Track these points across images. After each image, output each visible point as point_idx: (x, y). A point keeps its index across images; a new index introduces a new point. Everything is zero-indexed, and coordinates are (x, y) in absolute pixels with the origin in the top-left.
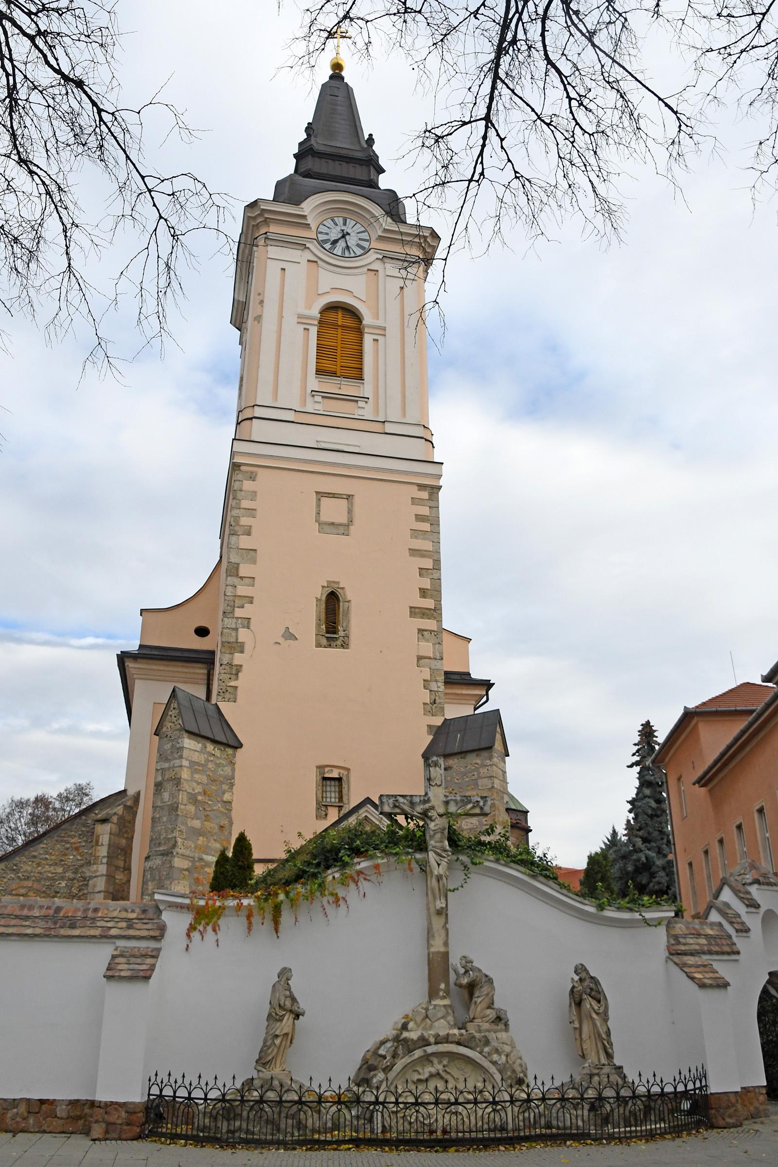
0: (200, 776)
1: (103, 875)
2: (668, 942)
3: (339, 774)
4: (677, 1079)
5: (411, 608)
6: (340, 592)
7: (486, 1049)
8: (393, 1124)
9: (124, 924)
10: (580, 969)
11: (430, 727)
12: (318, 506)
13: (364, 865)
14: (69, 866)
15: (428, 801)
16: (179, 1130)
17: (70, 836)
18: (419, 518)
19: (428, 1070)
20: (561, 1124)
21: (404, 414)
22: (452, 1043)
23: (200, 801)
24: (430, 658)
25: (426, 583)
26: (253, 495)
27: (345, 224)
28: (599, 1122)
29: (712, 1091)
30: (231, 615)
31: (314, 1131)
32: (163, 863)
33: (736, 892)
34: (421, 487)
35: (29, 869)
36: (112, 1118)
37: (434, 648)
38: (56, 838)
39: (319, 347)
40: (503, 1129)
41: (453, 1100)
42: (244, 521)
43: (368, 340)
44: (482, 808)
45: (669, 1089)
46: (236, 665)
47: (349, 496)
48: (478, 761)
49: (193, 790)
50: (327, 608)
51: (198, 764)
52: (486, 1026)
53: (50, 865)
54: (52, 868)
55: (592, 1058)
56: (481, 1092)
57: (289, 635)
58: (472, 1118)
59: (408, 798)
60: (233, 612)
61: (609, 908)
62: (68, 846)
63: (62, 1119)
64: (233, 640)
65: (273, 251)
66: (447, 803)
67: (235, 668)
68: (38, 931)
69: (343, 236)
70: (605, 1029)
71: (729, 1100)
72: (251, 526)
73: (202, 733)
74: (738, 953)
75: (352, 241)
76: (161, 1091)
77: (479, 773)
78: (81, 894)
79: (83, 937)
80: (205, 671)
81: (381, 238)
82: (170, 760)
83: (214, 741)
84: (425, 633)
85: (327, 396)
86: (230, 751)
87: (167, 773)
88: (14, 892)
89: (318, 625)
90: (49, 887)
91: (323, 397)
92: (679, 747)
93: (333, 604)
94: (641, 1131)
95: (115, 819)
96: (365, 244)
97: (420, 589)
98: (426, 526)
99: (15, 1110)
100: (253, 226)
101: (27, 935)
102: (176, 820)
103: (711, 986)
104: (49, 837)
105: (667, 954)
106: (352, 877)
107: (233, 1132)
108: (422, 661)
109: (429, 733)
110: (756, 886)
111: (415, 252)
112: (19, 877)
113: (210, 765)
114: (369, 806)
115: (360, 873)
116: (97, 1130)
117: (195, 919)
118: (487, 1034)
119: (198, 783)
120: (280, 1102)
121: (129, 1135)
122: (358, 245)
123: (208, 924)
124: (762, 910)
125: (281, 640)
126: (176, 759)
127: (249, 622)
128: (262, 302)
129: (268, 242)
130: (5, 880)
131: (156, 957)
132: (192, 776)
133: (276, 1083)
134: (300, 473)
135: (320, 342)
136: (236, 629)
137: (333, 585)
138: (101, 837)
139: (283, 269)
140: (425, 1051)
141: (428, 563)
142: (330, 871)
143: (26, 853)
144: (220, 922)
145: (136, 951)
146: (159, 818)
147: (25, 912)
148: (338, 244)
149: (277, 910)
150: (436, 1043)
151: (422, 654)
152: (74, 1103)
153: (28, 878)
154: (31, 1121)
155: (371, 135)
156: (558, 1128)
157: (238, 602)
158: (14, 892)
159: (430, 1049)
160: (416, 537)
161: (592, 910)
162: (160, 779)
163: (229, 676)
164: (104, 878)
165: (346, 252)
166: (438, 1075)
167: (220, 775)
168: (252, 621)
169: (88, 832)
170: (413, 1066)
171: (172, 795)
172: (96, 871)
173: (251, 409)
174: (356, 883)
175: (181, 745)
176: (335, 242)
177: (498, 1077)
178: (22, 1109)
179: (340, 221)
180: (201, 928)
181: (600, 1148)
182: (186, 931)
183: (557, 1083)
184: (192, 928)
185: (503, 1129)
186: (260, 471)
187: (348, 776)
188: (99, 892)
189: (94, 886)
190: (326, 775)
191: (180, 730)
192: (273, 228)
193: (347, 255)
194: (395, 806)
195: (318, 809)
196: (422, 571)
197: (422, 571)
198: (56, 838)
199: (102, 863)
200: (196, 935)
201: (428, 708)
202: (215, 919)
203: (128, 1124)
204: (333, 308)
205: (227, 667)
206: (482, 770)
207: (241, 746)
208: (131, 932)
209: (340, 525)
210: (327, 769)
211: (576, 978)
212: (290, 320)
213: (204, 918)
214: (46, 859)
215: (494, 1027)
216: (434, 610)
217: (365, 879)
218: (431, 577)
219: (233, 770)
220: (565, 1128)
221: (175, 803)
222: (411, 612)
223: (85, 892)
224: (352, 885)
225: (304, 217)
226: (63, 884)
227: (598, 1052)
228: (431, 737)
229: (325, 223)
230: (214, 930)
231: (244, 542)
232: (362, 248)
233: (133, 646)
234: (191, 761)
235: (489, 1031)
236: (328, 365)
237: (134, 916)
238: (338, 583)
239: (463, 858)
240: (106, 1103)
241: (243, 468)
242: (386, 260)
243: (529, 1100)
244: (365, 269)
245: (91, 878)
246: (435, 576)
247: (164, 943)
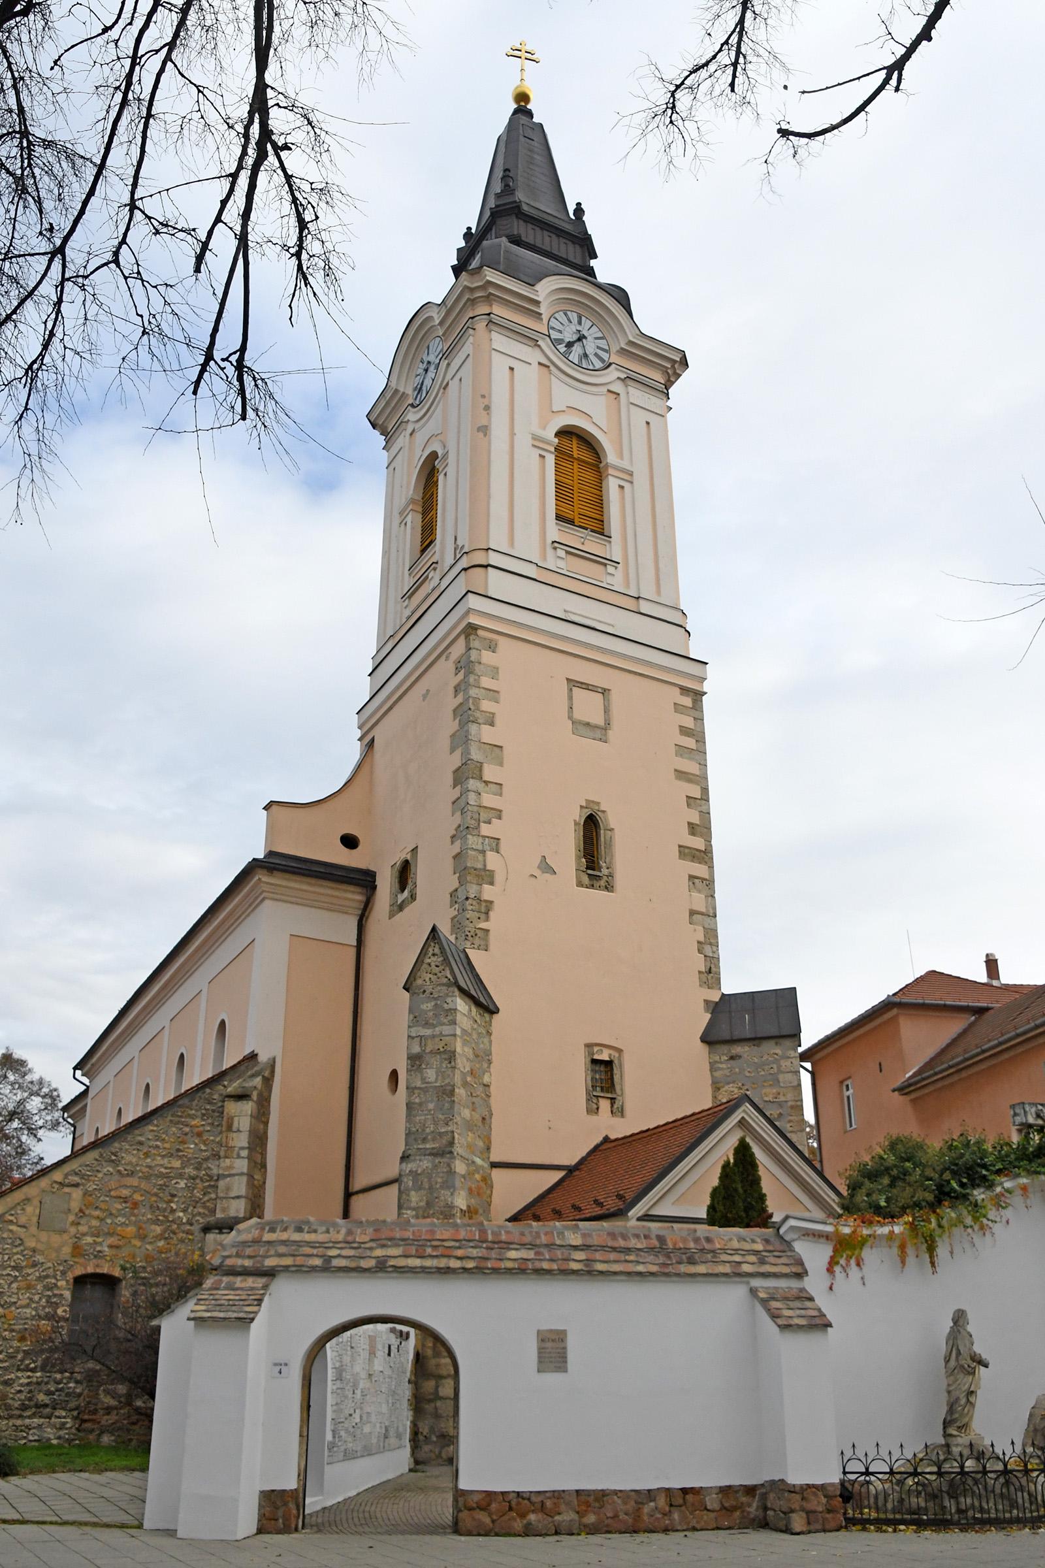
1: (242, 1174)
3: (610, 1056)
5: (680, 846)
9: (753, 1258)
12: (570, 698)
14: (189, 1159)
17: (190, 1116)
18: (684, 731)
21: (659, 592)
24: (702, 914)
25: (695, 818)
26: (494, 672)
27: (580, 323)
30: (475, 832)
32: (435, 1166)
34: (684, 690)
38: (170, 1118)
39: (558, 483)
42: (486, 705)
43: (612, 485)
46: (486, 901)
47: (605, 690)
48: (778, 1051)
53: (163, 1157)
54: (166, 1160)
57: (546, 867)
62: (187, 1129)
63: (713, 1511)
64: (480, 866)
65: (499, 341)
67: (484, 904)
68: (654, 1269)
69: (579, 339)
72: (493, 714)
75: (590, 346)
77: (779, 1067)
78: (206, 1198)
80: (361, 898)
81: (622, 352)
82: (434, 1026)
84: (696, 881)
85: (573, 552)
87: (429, 1041)
88: (113, 1193)
89: (578, 858)
90: (162, 1188)
91: (567, 552)
92: (859, 1037)
93: (591, 826)
95: (255, 1096)
96: (605, 356)
98: (690, 743)
99: (652, 1504)
101: (640, 1274)
102: (452, 1108)
104: (161, 1116)
108: (695, 917)
109: (707, 1010)
111: (659, 377)
112: (119, 1171)
116: (798, 1521)
117: (835, 1250)
121: (832, 1525)
122: (596, 355)
125: (537, 873)
126: (444, 1024)
127: (497, 845)
128: (487, 408)
129: (492, 326)
130: (100, 1175)
134: (547, 651)
136: (483, 852)
137: (591, 805)
138: (236, 1119)
139: (512, 369)
141: (696, 792)
143: (129, 1137)
146: (420, 1104)
147: (621, 1243)
148: (574, 348)
151: (695, 908)
152: (726, 1490)
153: (132, 1174)
154: (676, 1516)
155: (579, 204)
157: (484, 816)
158: (113, 1193)
160: (681, 756)
162: (416, 1049)
163: (478, 915)
164: (245, 1179)
168: (502, 843)
169: (213, 1111)
172: (231, 1167)
173: (483, 553)
175: (451, 1006)
176: (570, 345)
178: (662, 1502)
179: (574, 317)
186: (502, 641)
188: (238, 1197)
189: (228, 1189)
190: (596, 1057)
191: (448, 985)
192: (498, 310)
195: (588, 1100)
198: (170, 1118)
199: (239, 1157)
202: (856, 1252)
203: (829, 1511)
204: (566, 433)
205: (474, 903)
207: (497, 1011)
208: (767, 1268)
209: (596, 727)
210: (596, 1049)
212: (523, 443)
213: (845, 1250)
214: (157, 1147)
221: (448, 1084)
223: (213, 1196)
225: (537, 303)
226: (182, 1184)
230: (858, 1265)
231: (487, 734)
232: (602, 360)
234: (463, 1030)
238: (598, 803)
240: (801, 1486)
241: (480, 632)
242: (630, 382)
244: (604, 389)
245: (219, 1177)
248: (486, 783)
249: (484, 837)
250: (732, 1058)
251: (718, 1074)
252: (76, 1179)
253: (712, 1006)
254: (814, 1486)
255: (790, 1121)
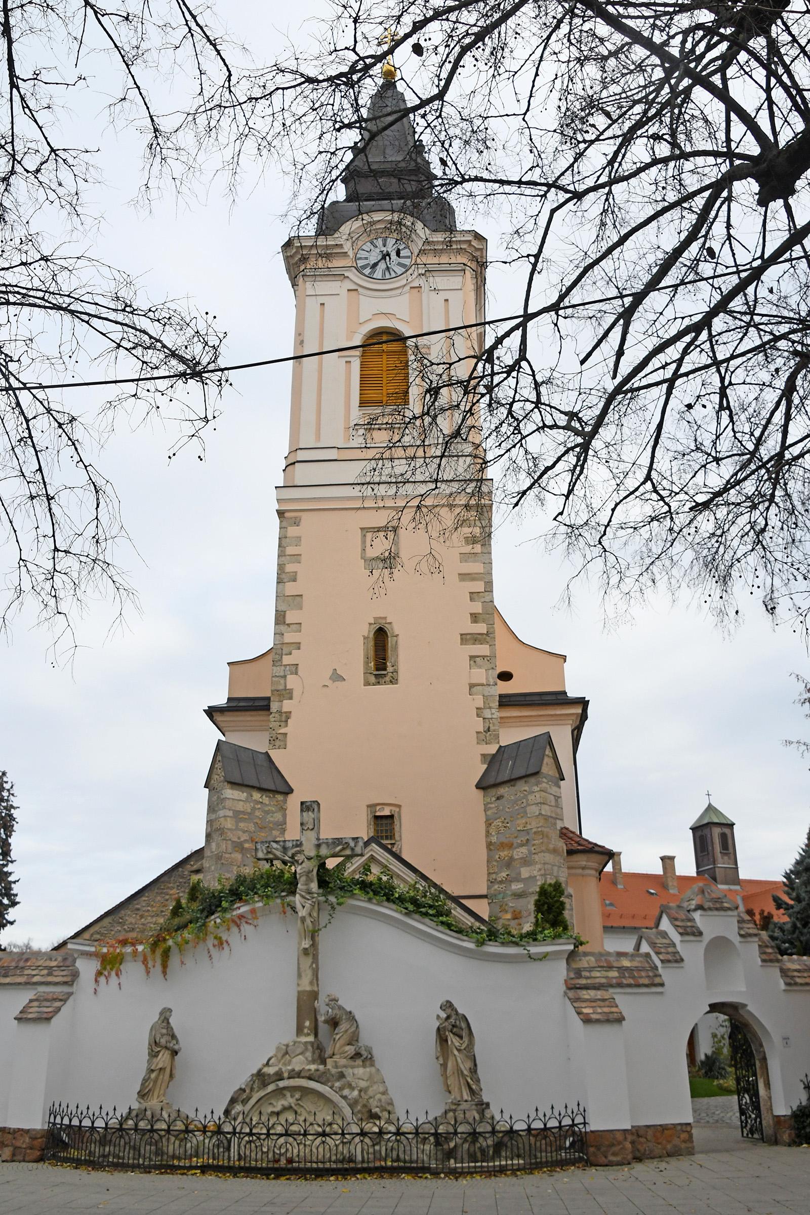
0: (246, 824)
2: (568, 975)
4: (532, 1117)
5: (462, 635)
6: (387, 628)
7: (337, 1084)
8: (248, 1153)
10: (448, 1006)
11: (483, 756)
13: (243, 909)
15: (301, 845)
16: (141, 1161)
17: (168, 888)
19: (279, 1105)
20: (407, 1158)
22: (303, 1078)
23: (246, 849)
24: (483, 685)
25: (478, 608)
28: (440, 1156)
29: (593, 1129)
30: (279, 663)
31: (174, 1157)
33: (673, 919)
35: (133, 921)
36: (19, 1143)
37: (487, 674)
40: (351, 1160)
41: (302, 1132)
44: (353, 849)
45: (553, 1123)
46: (286, 712)
48: (526, 788)
49: (239, 838)
50: (376, 645)
51: (243, 813)
52: (343, 1062)
54: (154, 919)
55: (455, 1095)
56: (330, 1124)
57: (337, 677)
58: (316, 1150)
59: (281, 843)
60: (281, 660)
61: (491, 943)
62: (167, 897)
64: (281, 687)
66: (318, 846)
67: (284, 715)
70: (469, 1064)
71: (614, 1138)
72: (296, 572)
73: (245, 783)
74: (662, 985)
76: (80, 1122)
79: (11, 984)
83: (261, 789)
84: (478, 659)
86: (280, 797)
89: (366, 663)
93: (381, 638)
94: (512, 1164)
97: (471, 614)
100: (293, 264)
103: (598, 1021)
105: (564, 988)
106: (233, 921)
107: (104, 1156)
109: (483, 762)
110: (699, 912)
113: (257, 813)
114: (374, 845)
115: (241, 917)
118: (344, 1070)
119: (244, 832)
120: (152, 1131)
121: (31, 1157)
123: (111, 969)
124: (708, 936)
125: (329, 683)
131: (65, 1001)
132: (237, 826)
133: (149, 1113)
134: (331, 512)
135: (364, 372)
136: (285, 677)
137: (380, 621)
140: (277, 1085)
141: (479, 586)
142: (213, 917)
143: (131, 906)
144: (122, 967)
145: (46, 996)
148: (378, 267)
149: (166, 954)
150: (289, 1078)
151: (474, 681)
153: (133, 930)
156: (405, 1162)
157: (285, 650)
159: (281, 1084)
160: (466, 561)
161: (471, 946)
165: (387, 273)
166: (290, 1108)
167: (270, 822)
170: (268, 1099)
171: (218, 846)
174: (238, 926)
176: (375, 265)
177: (347, 1111)
179: (380, 242)
180: (106, 973)
181: (439, 1181)
182: (94, 977)
183: (431, 1118)
184: (99, 974)
185: (351, 1160)
187: (399, 813)
190: (378, 814)
193: (388, 276)
194: (268, 852)
196: (473, 596)
197: (473, 596)
200: (102, 979)
201: (482, 736)
202: (117, 965)
203: (31, 1149)
205: (277, 715)
206: (531, 797)
207: (291, 791)
208: (50, 979)
210: (378, 808)
211: (443, 1015)
215: (351, 1063)
216: (487, 634)
217: (246, 922)
218: (483, 600)
219: (285, 816)
220: (411, 1162)
222: (462, 639)
224: (235, 929)
225: (341, 246)
227: (460, 1089)
228: (485, 766)
229: (364, 247)
230: (117, 975)
233: (221, 700)
234: (234, 811)
235: (345, 1066)
236: (372, 395)
237: (54, 964)
238: (385, 618)
239: (332, 899)
240: (14, 1129)
241: (287, 515)
243: (381, 1133)
244: (407, 288)
246: (487, 599)
247: (74, 988)
248: (288, 625)
249: (286, 665)
250: (498, 799)
251: (489, 813)
252: (98, 937)
253: (489, 759)
254: (22, 1130)
255: (534, 845)
